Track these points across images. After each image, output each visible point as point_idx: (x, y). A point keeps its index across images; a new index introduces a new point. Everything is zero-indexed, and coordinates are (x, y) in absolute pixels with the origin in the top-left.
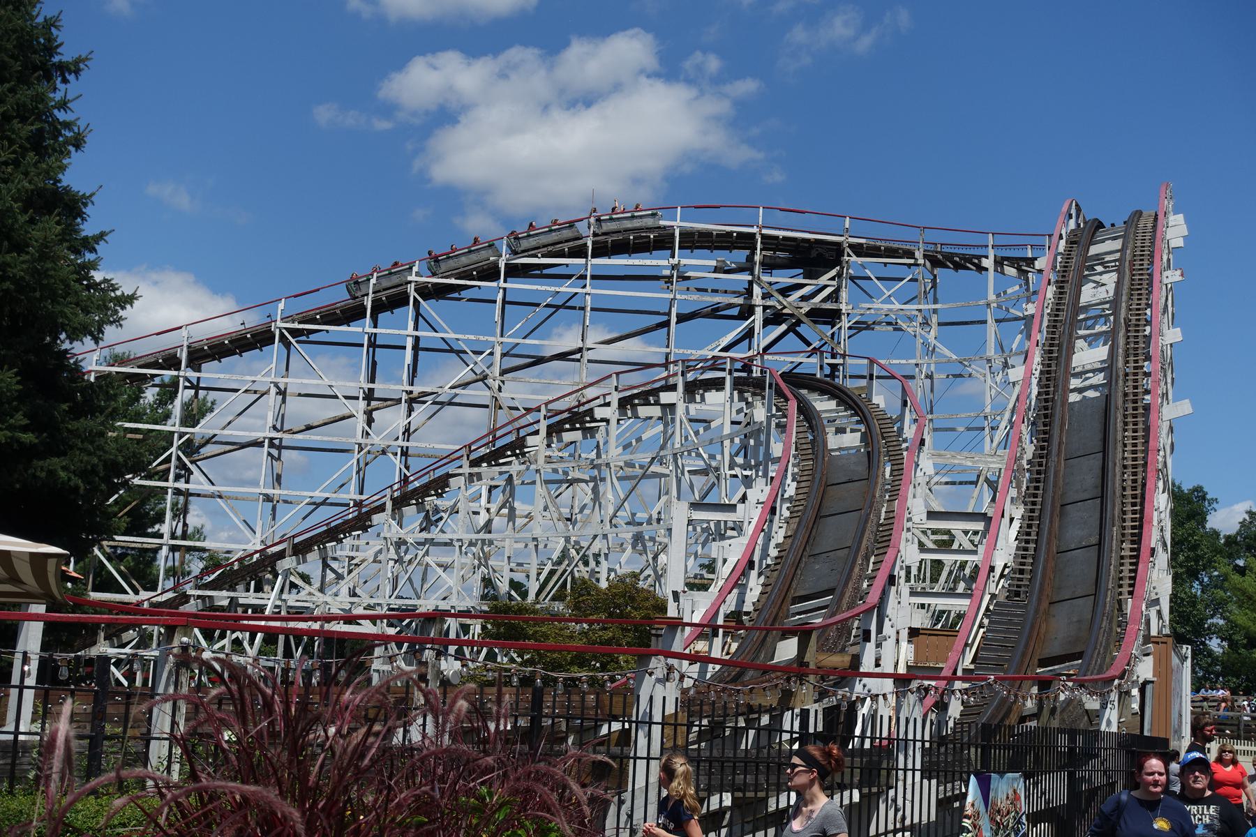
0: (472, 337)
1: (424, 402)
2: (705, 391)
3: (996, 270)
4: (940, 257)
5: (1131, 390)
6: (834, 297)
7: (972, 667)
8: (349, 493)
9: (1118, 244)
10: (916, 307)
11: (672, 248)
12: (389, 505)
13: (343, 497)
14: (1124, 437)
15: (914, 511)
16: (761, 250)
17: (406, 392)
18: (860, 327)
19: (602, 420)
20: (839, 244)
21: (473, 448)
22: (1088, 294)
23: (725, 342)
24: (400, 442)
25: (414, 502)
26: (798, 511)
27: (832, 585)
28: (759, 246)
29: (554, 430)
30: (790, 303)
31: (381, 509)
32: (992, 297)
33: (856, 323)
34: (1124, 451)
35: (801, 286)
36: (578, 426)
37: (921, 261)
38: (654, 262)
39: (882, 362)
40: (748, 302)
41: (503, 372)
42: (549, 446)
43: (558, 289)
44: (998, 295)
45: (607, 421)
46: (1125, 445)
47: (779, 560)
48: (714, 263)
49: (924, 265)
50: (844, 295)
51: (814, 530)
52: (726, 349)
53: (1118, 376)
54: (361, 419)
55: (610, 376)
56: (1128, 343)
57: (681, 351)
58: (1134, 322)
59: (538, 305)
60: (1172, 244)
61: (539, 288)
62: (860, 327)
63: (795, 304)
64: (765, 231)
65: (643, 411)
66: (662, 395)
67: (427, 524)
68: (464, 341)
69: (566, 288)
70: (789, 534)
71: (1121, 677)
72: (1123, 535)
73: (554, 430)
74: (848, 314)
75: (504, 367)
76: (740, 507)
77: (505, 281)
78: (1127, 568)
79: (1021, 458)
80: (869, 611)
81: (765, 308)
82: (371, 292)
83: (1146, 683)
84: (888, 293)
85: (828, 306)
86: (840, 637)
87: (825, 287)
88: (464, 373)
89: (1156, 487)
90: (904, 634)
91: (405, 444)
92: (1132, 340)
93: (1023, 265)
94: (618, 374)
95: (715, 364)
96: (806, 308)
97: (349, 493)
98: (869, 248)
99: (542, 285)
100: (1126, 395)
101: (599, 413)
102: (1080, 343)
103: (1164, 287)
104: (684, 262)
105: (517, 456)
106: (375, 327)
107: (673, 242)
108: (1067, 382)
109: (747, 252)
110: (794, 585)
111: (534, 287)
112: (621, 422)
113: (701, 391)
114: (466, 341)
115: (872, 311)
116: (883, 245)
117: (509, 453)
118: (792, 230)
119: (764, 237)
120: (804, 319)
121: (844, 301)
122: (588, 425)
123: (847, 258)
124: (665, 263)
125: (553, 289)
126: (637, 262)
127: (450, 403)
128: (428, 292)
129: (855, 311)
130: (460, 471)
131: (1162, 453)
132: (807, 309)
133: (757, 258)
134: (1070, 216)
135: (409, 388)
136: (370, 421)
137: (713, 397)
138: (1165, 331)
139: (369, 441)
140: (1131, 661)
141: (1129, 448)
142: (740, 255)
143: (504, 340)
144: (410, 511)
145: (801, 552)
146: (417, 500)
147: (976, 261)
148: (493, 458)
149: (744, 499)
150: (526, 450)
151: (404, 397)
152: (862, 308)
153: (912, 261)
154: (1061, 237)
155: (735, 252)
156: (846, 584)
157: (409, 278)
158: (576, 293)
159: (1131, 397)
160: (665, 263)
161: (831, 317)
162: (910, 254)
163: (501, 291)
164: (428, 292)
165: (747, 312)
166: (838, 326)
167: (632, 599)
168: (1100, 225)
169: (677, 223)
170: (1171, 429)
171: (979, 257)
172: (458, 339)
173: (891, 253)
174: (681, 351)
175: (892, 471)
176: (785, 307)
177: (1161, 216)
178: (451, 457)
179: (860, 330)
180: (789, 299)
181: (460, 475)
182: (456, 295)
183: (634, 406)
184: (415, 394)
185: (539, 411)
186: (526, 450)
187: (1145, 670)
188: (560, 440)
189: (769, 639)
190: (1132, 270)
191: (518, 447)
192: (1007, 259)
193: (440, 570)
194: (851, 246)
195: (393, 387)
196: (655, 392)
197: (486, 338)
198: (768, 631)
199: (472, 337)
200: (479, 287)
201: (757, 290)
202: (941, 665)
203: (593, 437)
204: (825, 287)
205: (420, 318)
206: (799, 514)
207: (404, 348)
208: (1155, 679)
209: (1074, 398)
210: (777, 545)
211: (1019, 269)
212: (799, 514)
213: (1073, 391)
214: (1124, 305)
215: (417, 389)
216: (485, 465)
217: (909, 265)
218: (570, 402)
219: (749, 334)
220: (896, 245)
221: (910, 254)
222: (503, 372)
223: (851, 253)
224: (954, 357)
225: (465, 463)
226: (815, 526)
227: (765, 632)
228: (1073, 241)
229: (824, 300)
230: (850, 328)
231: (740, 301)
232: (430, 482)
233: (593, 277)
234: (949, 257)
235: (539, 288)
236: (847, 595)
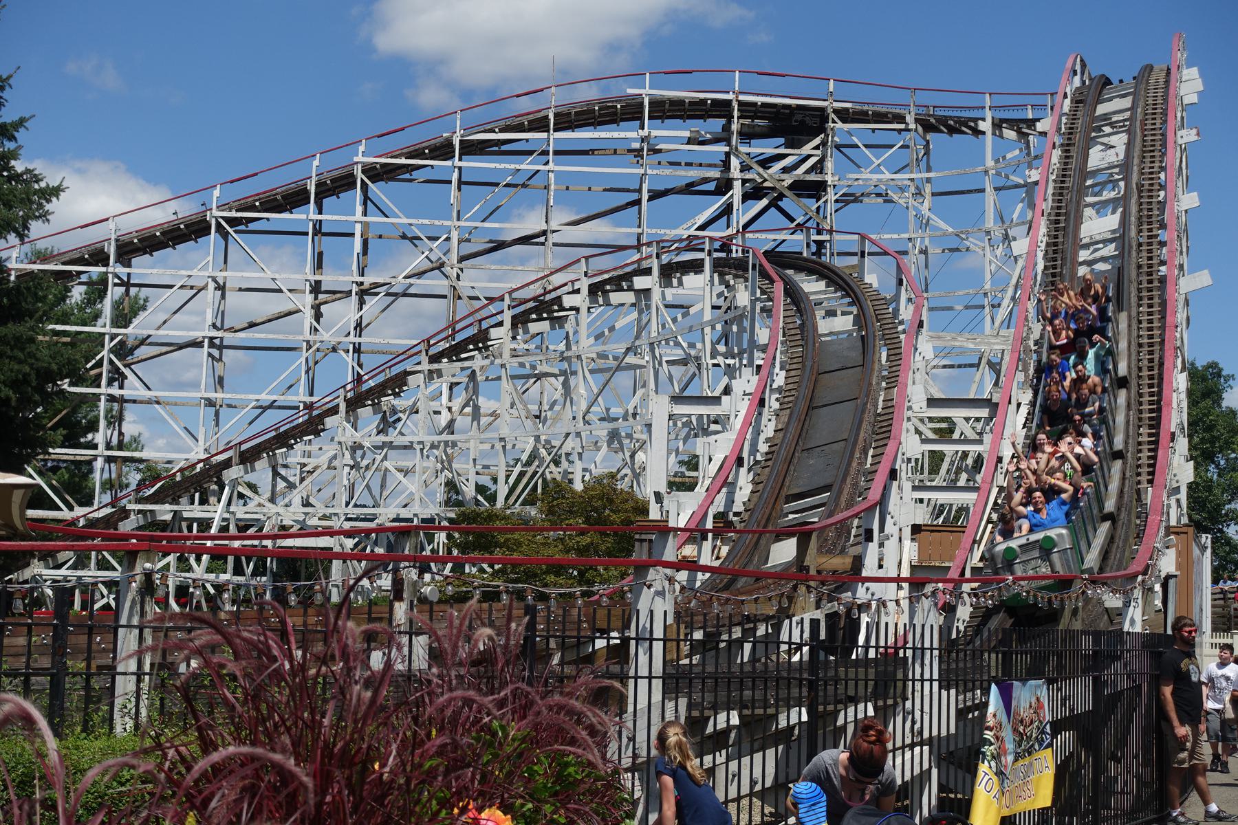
0: (426, 222)
1: (376, 294)
2: (683, 274)
3: (994, 134)
4: (932, 120)
5: (1146, 262)
6: (819, 167)
7: (981, 565)
8: (297, 394)
9: (1127, 102)
10: (907, 176)
11: (641, 119)
12: (343, 407)
13: (291, 399)
14: (1139, 313)
15: (914, 399)
16: (738, 118)
17: (357, 283)
18: (848, 199)
19: (571, 309)
20: (822, 110)
21: (432, 342)
22: (1096, 158)
23: (701, 219)
24: (352, 338)
25: (370, 402)
26: (788, 402)
27: (828, 482)
28: (736, 114)
29: (520, 321)
30: (771, 176)
31: (334, 411)
32: (990, 163)
33: (844, 195)
34: (1139, 329)
35: (782, 157)
36: (545, 315)
37: (912, 126)
38: (622, 135)
39: (873, 237)
40: (726, 176)
41: (462, 259)
42: (514, 338)
43: (518, 167)
44: (997, 161)
45: (577, 310)
46: (1140, 322)
47: (770, 456)
48: (687, 134)
49: (916, 130)
50: (829, 165)
51: (807, 422)
52: (702, 228)
53: (1130, 247)
54: (309, 313)
55: (579, 260)
56: (1140, 210)
57: (654, 231)
58: (1147, 187)
59: (497, 185)
60: (1186, 101)
61: (498, 166)
62: (848, 199)
63: (777, 177)
64: (741, 98)
65: (615, 298)
66: (635, 279)
67: (386, 425)
68: (417, 226)
69: (527, 165)
70: (780, 427)
71: (1145, 573)
72: (1140, 419)
73: (520, 321)
74: (834, 186)
75: (463, 253)
76: (724, 398)
77: (460, 159)
78: (1145, 454)
79: (1028, 338)
80: (871, 509)
81: (744, 181)
82: (314, 175)
83: (1169, 577)
84: (877, 162)
85: (812, 177)
86: (839, 537)
87: (809, 156)
88: (418, 261)
89: (1175, 366)
90: (907, 532)
91: (357, 340)
92: (1145, 206)
93: (1023, 127)
94: (587, 258)
95: (691, 244)
96: (788, 180)
97: (297, 394)
98: (856, 112)
99: (500, 162)
100: (1139, 267)
101: (568, 301)
102: (1088, 212)
103: (1178, 148)
104: (654, 133)
105: (479, 349)
106: (320, 213)
107: (642, 112)
108: (1076, 255)
109: (723, 121)
110: (787, 482)
111: (492, 165)
112: (592, 310)
113: (678, 275)
114: (419, 226)
115: (861, 182)
116: (870, 109)
117: (471, 347)
118: (771, 96)
119: (741, 103)
120: (787, 193)
121: (829, 172)
122: (556, 314)
123: (832, 125)
124: (633, 135)
125: (513, 166)
126: (603, 135)
127: (405, 295)
128: (377, 174)
129: (841, 183)
130: (419, 368)
131: (1179, 329)
132: (790, 182)
133: (735, 127)
134: (1075, 73)
135: (360, 279)
136: (318, 316)
137: (692, 281)
138: (1180, 196)
139: (317, 338)
140: (1154, 554)
141: (1145, 325)
142: (716, 125)
143: (462, 223)
144: (365, 412)
145: (793, 445)
146: (373, 400)
147: (972, 124)
148: (454, 353)
149: (727, 391)
150: (489, 343)
151: (355, 289)
152: (849, 179)
153: (902, 126)
154: (1065, 96)
155: (710, 121)
156: (844, 480)
157: (356, 159)
158: (538, 171)
159: (1146, 269)
160: (633, 135)
161: (815, 189)
162: (900, 119)
163: (456, 170)
164: (377, 174)
165: (724, 186)
166: (823, 200)
167: (611, 501)
168: (1108, 82)
169: (647, 91)
170: (1187, 302)
171: (976, 120)
172: (411, 225)
173: (880, 117)
174: (654, 231)
175: (888, 356)
176: (765, 180)
177: (1174, 71)
178: (408, 353)
179: (847, 203)
180: (770, 171)
181: (419, 372)
182: (407, 176)
183: (605, 293)
184: (366, 286)
185: (503, 300)
186: (489, 343)
187: (1168, 564)
188: (526, 331)
189: (763, 542)
190: (1143, 130)
191: (481, 340)
192: (1006, 121)
193: (400, 476)
194: (836, 111)
195: (342, 278)
196: (628, 277)
197: (441, 222)
198: (761, 533)
199: (426, 222)
200: (432, 167)
201: (735, 163)
202: (947, 564)
203: (561, 327)
204: (809, 156)
205: (369, 202)
206: (790, 405)
207: (352, 235)
208: (1178, 573)
209: (1082, 271)
210: (768, 440)
211: (1019, 132)
212: (790, 405)
213: (1082, 264)
214: (1135, 168)
215: (368, 280)
216: (445, 360)
217: (900, 131)
218: (535, 290)
219: (727, 210)
220: (884, 109)
221: (900, 119)
222: (462, 259)
223: (836, 119)
224: (950, 230)
225: (424, 358)
226: (808, 418)
227: (757, 535)
228: (1079, 100)
229: (808, 172)
230: (837, 201)
231: (715, 173)
232: (387, 381)
233: (556, 153)
234: (943, 120)
235: (498, 166)
236: (846, 491)
